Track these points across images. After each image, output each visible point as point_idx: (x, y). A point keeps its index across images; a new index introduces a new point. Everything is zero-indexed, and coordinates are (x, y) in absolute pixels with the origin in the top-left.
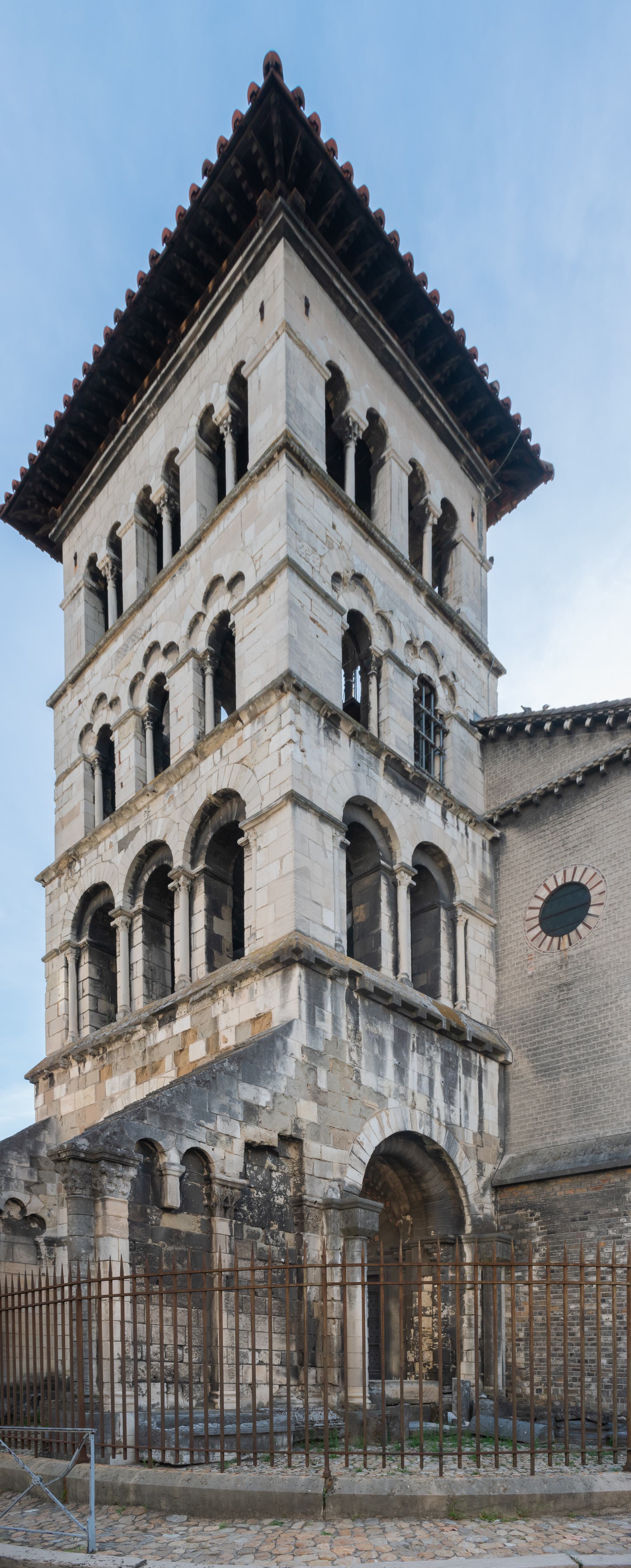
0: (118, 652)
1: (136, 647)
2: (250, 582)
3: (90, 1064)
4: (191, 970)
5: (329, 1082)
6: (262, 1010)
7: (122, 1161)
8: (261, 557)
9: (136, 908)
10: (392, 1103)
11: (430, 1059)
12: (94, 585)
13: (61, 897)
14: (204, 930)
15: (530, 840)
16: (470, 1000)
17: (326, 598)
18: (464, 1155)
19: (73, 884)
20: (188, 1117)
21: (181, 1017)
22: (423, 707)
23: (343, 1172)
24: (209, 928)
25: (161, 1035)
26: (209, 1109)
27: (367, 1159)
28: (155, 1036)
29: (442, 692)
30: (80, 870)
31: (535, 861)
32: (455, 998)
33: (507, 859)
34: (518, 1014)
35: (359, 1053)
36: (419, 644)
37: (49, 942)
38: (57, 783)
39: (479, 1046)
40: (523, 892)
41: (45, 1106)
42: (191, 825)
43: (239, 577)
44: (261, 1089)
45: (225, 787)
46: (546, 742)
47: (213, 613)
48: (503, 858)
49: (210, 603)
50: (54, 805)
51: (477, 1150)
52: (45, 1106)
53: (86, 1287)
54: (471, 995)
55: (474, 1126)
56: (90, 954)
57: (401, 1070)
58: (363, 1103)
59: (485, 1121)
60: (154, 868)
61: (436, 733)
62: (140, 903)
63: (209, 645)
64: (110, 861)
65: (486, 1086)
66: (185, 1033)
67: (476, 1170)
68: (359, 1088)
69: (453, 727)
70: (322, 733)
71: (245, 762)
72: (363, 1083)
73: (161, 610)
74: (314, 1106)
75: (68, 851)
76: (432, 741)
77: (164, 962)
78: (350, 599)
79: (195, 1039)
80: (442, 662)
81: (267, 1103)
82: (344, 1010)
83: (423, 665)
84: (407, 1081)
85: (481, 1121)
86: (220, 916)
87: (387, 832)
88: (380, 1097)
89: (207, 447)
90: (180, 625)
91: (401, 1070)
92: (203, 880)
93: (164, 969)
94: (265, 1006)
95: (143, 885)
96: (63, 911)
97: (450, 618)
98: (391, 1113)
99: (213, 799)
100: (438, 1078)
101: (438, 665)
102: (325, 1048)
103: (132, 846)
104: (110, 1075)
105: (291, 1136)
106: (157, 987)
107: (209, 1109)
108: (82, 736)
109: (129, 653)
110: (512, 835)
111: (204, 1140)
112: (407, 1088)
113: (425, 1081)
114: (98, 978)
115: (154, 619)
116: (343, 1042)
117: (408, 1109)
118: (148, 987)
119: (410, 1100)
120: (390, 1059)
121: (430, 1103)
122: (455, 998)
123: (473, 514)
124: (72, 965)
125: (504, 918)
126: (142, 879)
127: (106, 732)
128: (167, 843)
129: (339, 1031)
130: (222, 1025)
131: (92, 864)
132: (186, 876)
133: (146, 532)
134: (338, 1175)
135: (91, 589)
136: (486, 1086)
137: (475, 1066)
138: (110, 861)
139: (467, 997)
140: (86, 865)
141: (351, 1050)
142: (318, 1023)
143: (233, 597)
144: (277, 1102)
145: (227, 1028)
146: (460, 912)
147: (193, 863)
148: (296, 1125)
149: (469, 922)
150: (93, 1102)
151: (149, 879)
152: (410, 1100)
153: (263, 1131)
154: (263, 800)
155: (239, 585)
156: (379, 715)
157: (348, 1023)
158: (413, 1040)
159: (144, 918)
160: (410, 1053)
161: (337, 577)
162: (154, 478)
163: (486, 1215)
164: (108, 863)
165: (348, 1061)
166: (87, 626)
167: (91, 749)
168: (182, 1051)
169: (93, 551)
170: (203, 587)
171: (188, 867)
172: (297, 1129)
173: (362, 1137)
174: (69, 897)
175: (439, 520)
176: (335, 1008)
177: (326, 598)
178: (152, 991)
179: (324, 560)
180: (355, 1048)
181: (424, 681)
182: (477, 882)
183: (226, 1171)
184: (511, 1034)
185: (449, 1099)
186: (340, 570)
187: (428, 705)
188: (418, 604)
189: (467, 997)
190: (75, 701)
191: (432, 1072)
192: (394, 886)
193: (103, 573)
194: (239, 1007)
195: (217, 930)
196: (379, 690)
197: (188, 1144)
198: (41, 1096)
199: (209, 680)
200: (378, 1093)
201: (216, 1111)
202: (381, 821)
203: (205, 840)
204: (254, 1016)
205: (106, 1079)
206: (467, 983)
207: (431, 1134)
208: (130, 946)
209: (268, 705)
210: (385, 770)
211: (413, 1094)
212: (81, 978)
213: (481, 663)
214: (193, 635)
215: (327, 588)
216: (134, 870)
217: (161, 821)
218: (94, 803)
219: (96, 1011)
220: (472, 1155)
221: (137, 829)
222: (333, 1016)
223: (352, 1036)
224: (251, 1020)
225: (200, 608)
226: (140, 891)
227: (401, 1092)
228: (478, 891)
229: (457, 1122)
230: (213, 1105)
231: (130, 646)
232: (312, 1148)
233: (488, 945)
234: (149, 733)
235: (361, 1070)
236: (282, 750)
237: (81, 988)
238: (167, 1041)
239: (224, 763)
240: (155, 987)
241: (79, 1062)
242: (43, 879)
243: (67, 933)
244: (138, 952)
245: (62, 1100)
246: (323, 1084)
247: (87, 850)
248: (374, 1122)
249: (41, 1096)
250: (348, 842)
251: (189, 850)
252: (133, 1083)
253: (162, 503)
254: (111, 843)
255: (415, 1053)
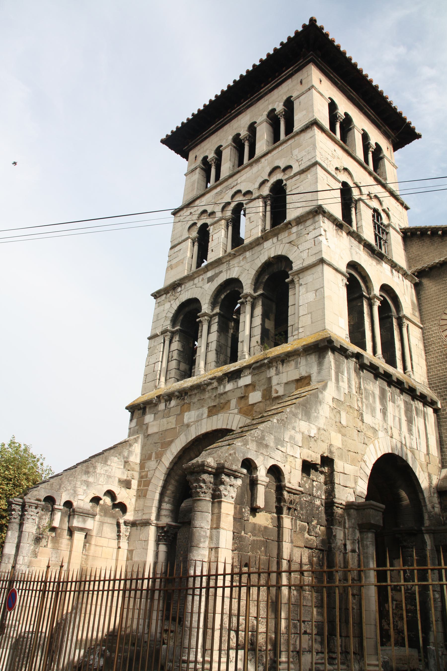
0: (217, 193)
1: (227, 192)
2: (296, 169)
3: (173, 403)
4: (250, 348)
5: (347, 421)
6: (304, 374)
7: (233, 474)
8: (302, 160)
9: (215, 312)
10: (381, 434)
11: (398, 406)
12: (204, 167)
13: (166, 305)
14: (260, 326)
15: (437, 285)
16: (414, 369)
17: (333, 176)
18: (420, 469)
19: (175, 298)
20: (272, 444)
21: (245, 376)
22: (376, 221)
23: (356, 482)
24: (263, 325)
25: (229, 387)
26: (283, 438)
27: (369, 472)
28: (225, 387)
29: (383, 215)
30: (180, 291)
31: (442, 295)
32: (405, 368)
33: (425, 293)
34: (442, 379)
35: (362, 402)
36: (372, 195)
37: (154, 328)
38: (172, 248)
39: (423, 398)
40: (437, 311)
41: (137, 428)
42: (256, 271)
43: (290, 167)
44: (311, 425)
45: (279, 253)
46: (440, 240)
47: (273, 180)
48: (422, 293)
49: (271, 176)
50: (167, 259)
51: (427, 466)
52: (137, 428)
53: (200, 580)
54: (414, 367)
55: (424, 450)
56: (179, 336)
57: (384, 412)
58: (365, 434)
59: (429, 446)
60: (228, 292)
61: (383, 233)
62: (217, 310)
63: (270, 192)
64: (201, 287)
65: (428, 423)
66: (246, 386)
67: (428, 480)
68: (363, 425)
69: (391, 231)
70: (335, 231)
71: (292, 243)
72: (365, 421)
73: (243, 178)
74: (339, 436)
75: (175, 281)
76: (381, 236)
77: (227, 343)
78: (344, 177)
79: (254, 390)
80: (383, 203)
81: (315, 434)
82: (353, 375)
83: (375, 204)
84: (387, 419)
85: (428, 446)
86: (269, 319)
87: (365, 278)
88: (375, 431)
89: (270, 121)
90: (254, 184)
91: (384, 412)
92: (261, 299)
93: (227, 346)
94: (306, 372)
95: (220, 300)
96: (166, 312)
97: (384, 186)
98: (380, 440)
99: (271, 260)
100: (404, 418)
101: (381, 204)
102: (345, 399)
103: (217, 281)
104: (189, 410)
105: (327, 457)
106: (222, 357)
107: (283, 438)
108: (190, 228)
109: (223, 194)
110: (426, 282)
111: (280, 460)
112: (388, 424)
113: (397, 419)
114: (182, 350)
115: (239, 181)
116: (354, 395)
117: (389, 438)
118: (217, 357)
119: (390, 433)
120: (378, 406)
121: (400, 435)
122: (405, 368)
123: (388, 148)
124: (167, 342)
125: (427, 324)
126: (220, 297)
127: (204, 227)
128: (241, 279)
129: (351, 388)
130: (275, 381)
131: (189, 288)
132: (251, 297)
133: (235, 149)
134: (353, 485)
135: (202, 169)
136: (428, 423)
137: (421, 411)
138: (201, 287)
139: (412, 368)
140: (185, 288)
141: (358, 400)
142: (341, 383)
143: (285, 174)
144: (320, 434)
145: (278, 384)
146: (404, 320)
147: (255, 290)
148: (330, 450)
149: (409, 326)
150: (174, 426)
151: (224, 298)
152: (390, 433)
153: (311, 452)
154: (304, 261)
155: (289, 170)
156: (357, 224)
157: (356, 383)
158: (389, 394)
159: (219, 318)
160: (388, 402)
161: (337, 169)
162: (242, 131)
163: (436, 514)
164: (200, 289)
165: (356, 408)
166: (198, 182)
167: (194, 234)
168: (244, 398)
169: (206, 155)
170: (268, 170)
171: (252, 292)
172: (331, 452)
173: (366, 458)
174: (171, 305)
175: (374, 150)
176: (349, 373)
177: (333, 176)
178: (219, 359)
179: (331, 162)
180: (359, 399)
181: (375, 210)
182: (410, 305)
183: (291, 481)
184: (438, 391)
185: (410, 430)
186: (338, 166)
187: (378, 220)
188: (371, 181)
189: (412, 368)
190: (188, 213)
191: (400, 415)
192: (371, 306)
193: (210, 163)
194: (287, 372)
195: (267, 326)
196: (356, 213)
197: (271, 462)
198: (135, 421)
199: (268, 208)
200: (373, 428)
201: (287, 439)
202: (363, 273)
203: (263, 278)
204: (298, 377)
205: (186, 412)
206: (411, 360)
207: (402, 455)
208: (209, 332)
209: (308, 218)
210: (363, 249)
211: (391, 428)
212: (172, 349)
213: (399, 204)
214: (261, 188)
215: (333, 172)
216: (216, 292)
217: (237, 269)
218: (192, 258)
219: (178, 369)
220: (425, 469)
221: (221, 272)
222: (348, 379)
223: (358, 392)
224: (296, 380)
225: (266, 177)
226: (218, 303)
227: (385, 427)
228: (411, 309)
229: (415, 447)
230: (285, 436)
231: (224, 191)
232: (339, 465)
233: (419, 339)
234: (230, 228)
235: (363, 413)
236: (316, 239)
237: (170, 355)
238: (233, 391)
239: (279, 243)
240: (221, 357)
241: (166, 401)
242: (156, 295)
243: (167, 324)
244: (214, 336)
245: (150, 424)
246: (344, 422)
247: (187, 281)
248: (371, 446)
249: (135, 421)
250: (348, 283)
251: (253, 284)
252: (205, 415)
253: (245, 139)
254: (203, 278)
255: (391, 402)
